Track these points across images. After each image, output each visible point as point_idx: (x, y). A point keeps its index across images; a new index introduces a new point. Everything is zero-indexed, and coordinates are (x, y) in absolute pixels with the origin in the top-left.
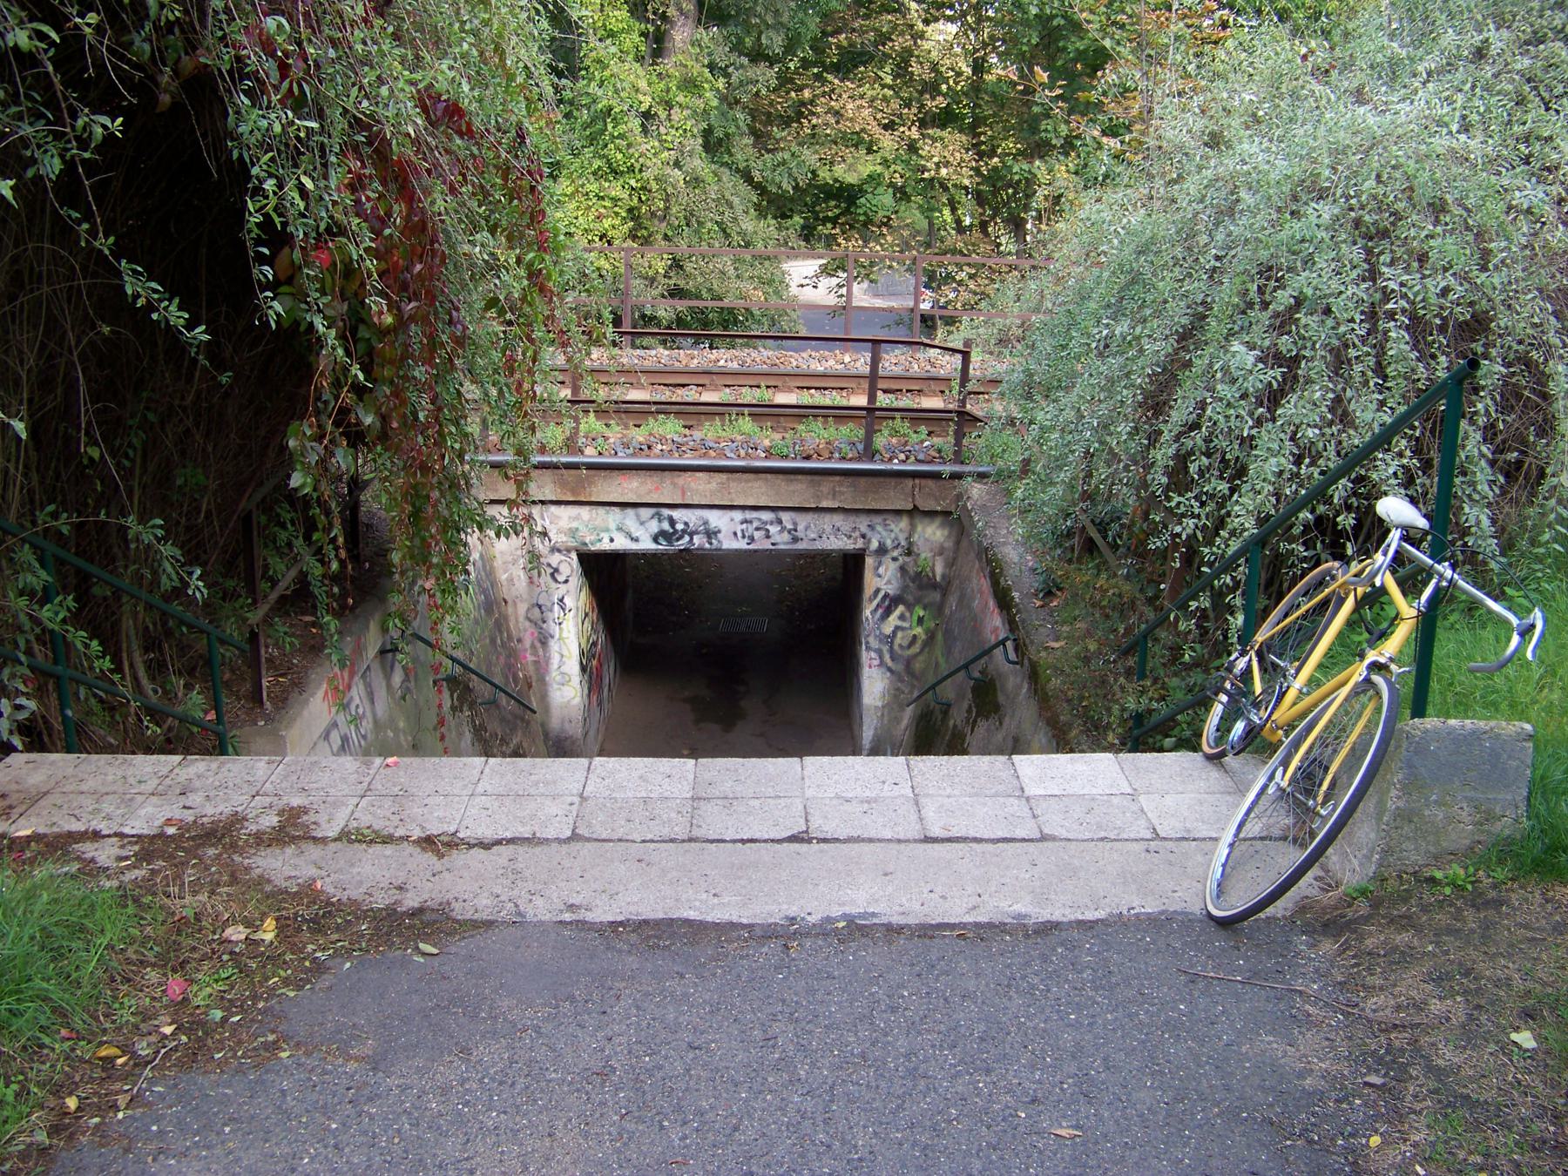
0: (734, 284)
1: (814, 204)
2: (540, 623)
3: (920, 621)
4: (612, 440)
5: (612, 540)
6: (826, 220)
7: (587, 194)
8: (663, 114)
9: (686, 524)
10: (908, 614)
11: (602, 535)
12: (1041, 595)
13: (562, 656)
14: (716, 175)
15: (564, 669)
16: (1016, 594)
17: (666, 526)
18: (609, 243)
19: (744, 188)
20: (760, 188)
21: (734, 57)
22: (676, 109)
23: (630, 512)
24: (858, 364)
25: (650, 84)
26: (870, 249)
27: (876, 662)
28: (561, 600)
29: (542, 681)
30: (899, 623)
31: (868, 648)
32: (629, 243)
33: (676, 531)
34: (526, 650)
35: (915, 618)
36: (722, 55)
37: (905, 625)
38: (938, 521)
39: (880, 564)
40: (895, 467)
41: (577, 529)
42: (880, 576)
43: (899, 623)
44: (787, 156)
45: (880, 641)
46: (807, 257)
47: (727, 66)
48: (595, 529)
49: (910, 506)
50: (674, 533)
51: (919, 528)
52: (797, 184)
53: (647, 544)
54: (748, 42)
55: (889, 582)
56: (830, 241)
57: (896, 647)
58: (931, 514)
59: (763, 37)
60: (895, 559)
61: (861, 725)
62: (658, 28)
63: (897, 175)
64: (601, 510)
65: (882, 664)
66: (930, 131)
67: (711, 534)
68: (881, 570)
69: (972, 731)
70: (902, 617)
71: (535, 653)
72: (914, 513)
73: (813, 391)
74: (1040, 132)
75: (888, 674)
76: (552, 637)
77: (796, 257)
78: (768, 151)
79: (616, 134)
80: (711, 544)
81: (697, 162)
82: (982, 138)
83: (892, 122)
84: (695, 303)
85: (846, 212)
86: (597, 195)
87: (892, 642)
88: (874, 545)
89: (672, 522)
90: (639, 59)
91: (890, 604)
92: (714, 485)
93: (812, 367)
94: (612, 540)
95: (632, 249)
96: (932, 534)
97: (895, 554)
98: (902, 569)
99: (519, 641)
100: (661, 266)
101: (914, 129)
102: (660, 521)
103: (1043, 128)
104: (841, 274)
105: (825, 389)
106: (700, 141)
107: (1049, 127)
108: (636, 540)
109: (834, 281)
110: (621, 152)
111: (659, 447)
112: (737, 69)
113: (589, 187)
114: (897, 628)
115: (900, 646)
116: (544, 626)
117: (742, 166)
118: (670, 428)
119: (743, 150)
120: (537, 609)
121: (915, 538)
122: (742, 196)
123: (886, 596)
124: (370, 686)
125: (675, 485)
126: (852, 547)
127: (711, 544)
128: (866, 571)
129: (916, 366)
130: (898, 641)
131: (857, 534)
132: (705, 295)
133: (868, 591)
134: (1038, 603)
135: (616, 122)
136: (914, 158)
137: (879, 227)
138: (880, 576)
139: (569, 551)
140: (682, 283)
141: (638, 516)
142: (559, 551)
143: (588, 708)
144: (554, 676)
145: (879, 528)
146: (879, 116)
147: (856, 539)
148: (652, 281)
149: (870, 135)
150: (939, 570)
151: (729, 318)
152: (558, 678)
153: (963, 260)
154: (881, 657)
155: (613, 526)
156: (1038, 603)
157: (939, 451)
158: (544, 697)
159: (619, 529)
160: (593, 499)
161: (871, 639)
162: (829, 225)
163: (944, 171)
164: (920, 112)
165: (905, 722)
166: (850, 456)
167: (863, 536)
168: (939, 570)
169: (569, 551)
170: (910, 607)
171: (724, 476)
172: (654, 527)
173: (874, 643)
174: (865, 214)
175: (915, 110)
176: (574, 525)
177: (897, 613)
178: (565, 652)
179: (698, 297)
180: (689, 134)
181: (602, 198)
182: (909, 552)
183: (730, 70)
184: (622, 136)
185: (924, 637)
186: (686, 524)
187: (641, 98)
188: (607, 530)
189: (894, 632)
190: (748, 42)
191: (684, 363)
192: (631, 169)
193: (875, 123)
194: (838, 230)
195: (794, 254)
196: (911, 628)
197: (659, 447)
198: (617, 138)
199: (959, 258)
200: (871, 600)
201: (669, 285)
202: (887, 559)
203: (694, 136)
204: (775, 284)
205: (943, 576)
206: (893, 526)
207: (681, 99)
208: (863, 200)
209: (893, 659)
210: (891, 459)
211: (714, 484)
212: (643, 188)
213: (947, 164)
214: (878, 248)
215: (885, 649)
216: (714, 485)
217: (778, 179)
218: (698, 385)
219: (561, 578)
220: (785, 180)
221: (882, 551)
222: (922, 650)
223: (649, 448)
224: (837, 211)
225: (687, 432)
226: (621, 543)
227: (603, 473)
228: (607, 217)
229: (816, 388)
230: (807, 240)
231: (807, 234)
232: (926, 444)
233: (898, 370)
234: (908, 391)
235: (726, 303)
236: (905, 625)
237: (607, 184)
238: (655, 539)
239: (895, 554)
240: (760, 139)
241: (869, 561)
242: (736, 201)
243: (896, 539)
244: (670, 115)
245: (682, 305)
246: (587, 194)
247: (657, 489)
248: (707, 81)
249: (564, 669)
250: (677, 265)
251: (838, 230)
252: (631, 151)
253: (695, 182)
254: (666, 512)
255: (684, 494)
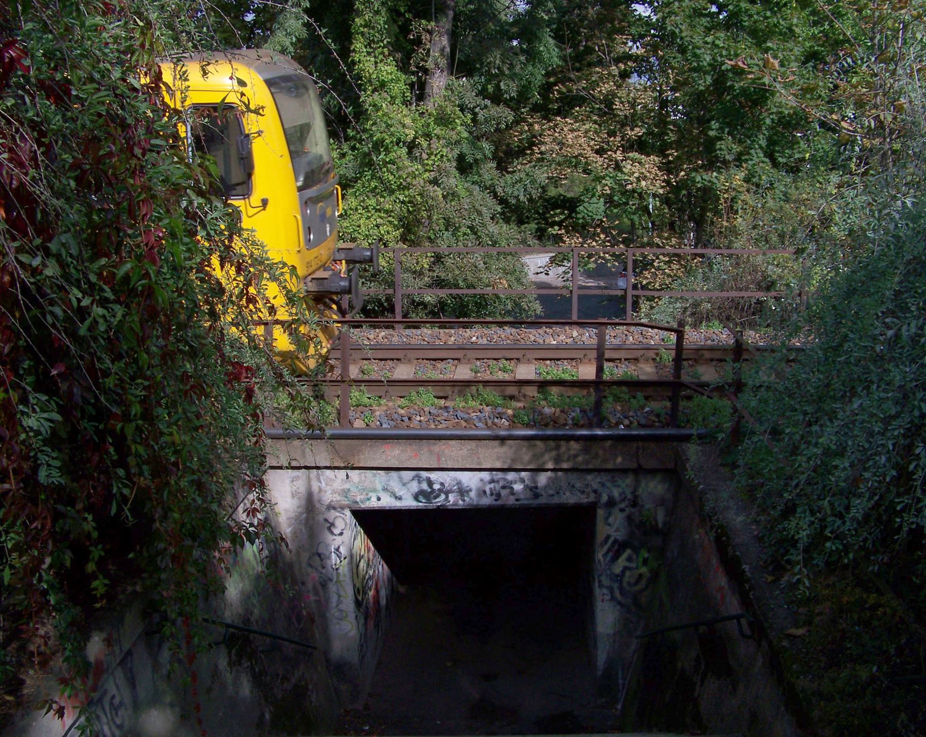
0: (485, 276)
1: (544, 213)
2: (320, 568)
3: (645, 562)
4: (378, 413)
5: (379, 499)
6: (553, 224)
7: (367, 207)
8: (425, 144)
9: (442, 484)
10: (634, 557)
11: (371, 494)
12: (770, 568)
13: (339, 596)
14: (468, 191)
15: (342, 607)
16: (746, 567)
17: (425, 486)
18: (385, 244)
19: (491, 202)
20: (503, 201)
21: (479, 100)
22: (434, 139)
23: (394, 474)
24: (584, 338)
25: (414, 121)
26: (588, 245)
27: (607, 597)
28: (338, 549)
29: (324, 617)
30: (627, 564)
31: (601, 586)
32: (401, 245)
33: (433, 491)
34: (308, 591)
35: (641, 559)
36: (471, 98)
37: (633, 565)
38: (659, 477)
39: (609, 515)
40: (621, 433)
41: (349, 490)
42: (609, 525)
43: (627, 564)
44: (523, 175)
45: (611, 579)
46: (539, 252)
47: (475, 107)
48: (364, 490)
49: (634, 465)
50: (431, 493)
51: (643, 484)
52: (531, 197)
53: (409, 503)
54: (490, 88)
55: (617, 530)
56: (558, 239)
57: (625, 584)
58: (652, 472)
59: (502, 84)
60: (622, 510)
61: (595, 646)
62: (419, 78)
63: (607, 188)
64: (369, 473)
65: (613, 598)
66: (630, 154)
67: (462, 491)
68: (611, 520)
69: (702, 681)
70: (629, 559)
71: (316, 593)
72: (639, 471)
73: (548, 362)
74: (716, 151)
75: (619, 607)
76: (331, 580)
77: (532, 253)
78: (508, 173)
79: (388, 160)
80: (464, 501)
81: (452, 181)
82: (670, 158)
83: (602, 148)
84: (455, 292)
85: (569, 216)
86: (374, 208)
87: (621, 581)
88: (605, 498)
89: (430, 483)
90: (406, 103)
91: (619, 548)
92: (465, 451)
93: (547, 341)
94: (379, 499)
95: (403, 249)
96: (654, 488)
97: (623, 505)
98: (629, 518)
99: (303, 583)
100: (425, 263)
101: (619, 152)
102: (419, 482)
103: (718, 147)
104: (565, 263)
105: (558, 360)
106: (454, 164)
107: (723, 147)
108: (399, 498)
109: (561, 269)
110: (392, 174)
111: (418, 418)
112: (482, 109)
113: (369, 202)
114: (625, 569)
115: (629, 583)
116: (324, 571)
117: (488, 183)
118: (427, 399)
119: (489, 170)
120: (317, 558)
121: (640, 492)
122: (491, 206)
123: (615, 541)
124: (131, 670)
125: (431, 452)
126: (586, 500)
127: (464, 501)
128: (598, 521)
129: (631, 338)
130: (626, 579)
131: (589, 489)
132: (461, 284)
133: (600, 538)
134: (770, 578)
135: (388, 152)
136: (619, 174)
137: (595, 228)
138: (609, 525)
139: (342, 508)
140: (443, 275)
141: (400, 478)
142: (334, 508)
143: (364, 637)
144: (334, 612)
145: (608, 484)
146: (592, 143)
147: (588, 494)
148: (419, 274)
149: (586, 158)
150: (661, 517)
151: (481, 303)
152: (337, 614)
153: (658, 251)
154: (612, 592)
155: (379, 487)
156: (770, 578)
157: (658, 416)
158: (325, 629)
159: (385, 489)
160: (361, 465)
161: (603, 578)
162: (556, 228)
163: (643, 183)
164: (623, 140)
165: (633, 647)
166: (582, 422)
167: (595, 492)
168: (661, 517)
169: (342, 508)
170: (636, 550)
171: (473, 444)
172: (414, 487)
173: (606, 581)
174: (583, 218)
175: (618, 139)
176: (347, 486)
177: (625, 556)
178: (342, 593)
179: (457, 286)
180: (445, 159)
181: (379, 211)
182: (634, 503)
183: (477, 110)
184: (393, 162)
185: (648, 575)
186: (442, 484)
187: (407, 131)
188: (375, 490)
189: (623, 572)
190: (490, 88)
191: (443, 340)
192: (402, 188)
193: (589, 149)
194: (563, 231)
195: (530, 249)
196: (637, 568)
197: (418, 418)
198: (389, 163)
199: (655, 250)
200: (602, 545)
201: (433, 277)
202: (616, 511)
203: (449, 160)
204: (516, 274)
205: (664, 523)
206: (620, 482)
207: (438, 131)
208: (581, 208)
209: (621, 593)
210: (617, 424)
211: (465, 450)
212: (410, 202)
213: (645, 178)
214: (594, 243)
215: (616, 586)
216: (465, 451)
217: (516, 193)
218: (453, 359)
219: (337, 531)
220: (522, 194)
221: (611, 503)
222: (647, 587)
223: (410, 419)
224: (562, 217)
225: (442, 402)
226: (387, 502)
227: (369, 442)
228: (384, 225)
229: (550, 360)
230: (540, 238)
231: (541, 235)
232: (647, 409)
233: (616, 342)
234: (625, 359)
235: (478, 291)
236: (633, 565)
237: (382, 200)
238: (416, 498)
239: (623, 505)
240: (502, 167)
241: (600, 513)
242: (484, 210)
243: (624, 493)
244: (430, 144)
245: (443, 293)
246: (367, 207)
247: (416, 455)
248: (459, 118)
249: (342, 607)
250: (438, 259)
251: (563, 231)
252: (400, 173)
253: (450, 196)
254: (424, 474)
255: (439, 459)
